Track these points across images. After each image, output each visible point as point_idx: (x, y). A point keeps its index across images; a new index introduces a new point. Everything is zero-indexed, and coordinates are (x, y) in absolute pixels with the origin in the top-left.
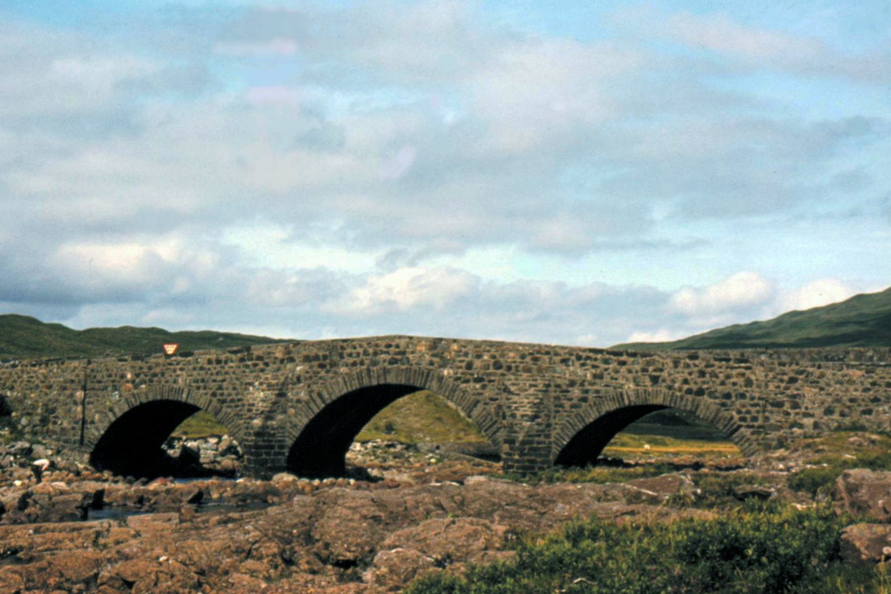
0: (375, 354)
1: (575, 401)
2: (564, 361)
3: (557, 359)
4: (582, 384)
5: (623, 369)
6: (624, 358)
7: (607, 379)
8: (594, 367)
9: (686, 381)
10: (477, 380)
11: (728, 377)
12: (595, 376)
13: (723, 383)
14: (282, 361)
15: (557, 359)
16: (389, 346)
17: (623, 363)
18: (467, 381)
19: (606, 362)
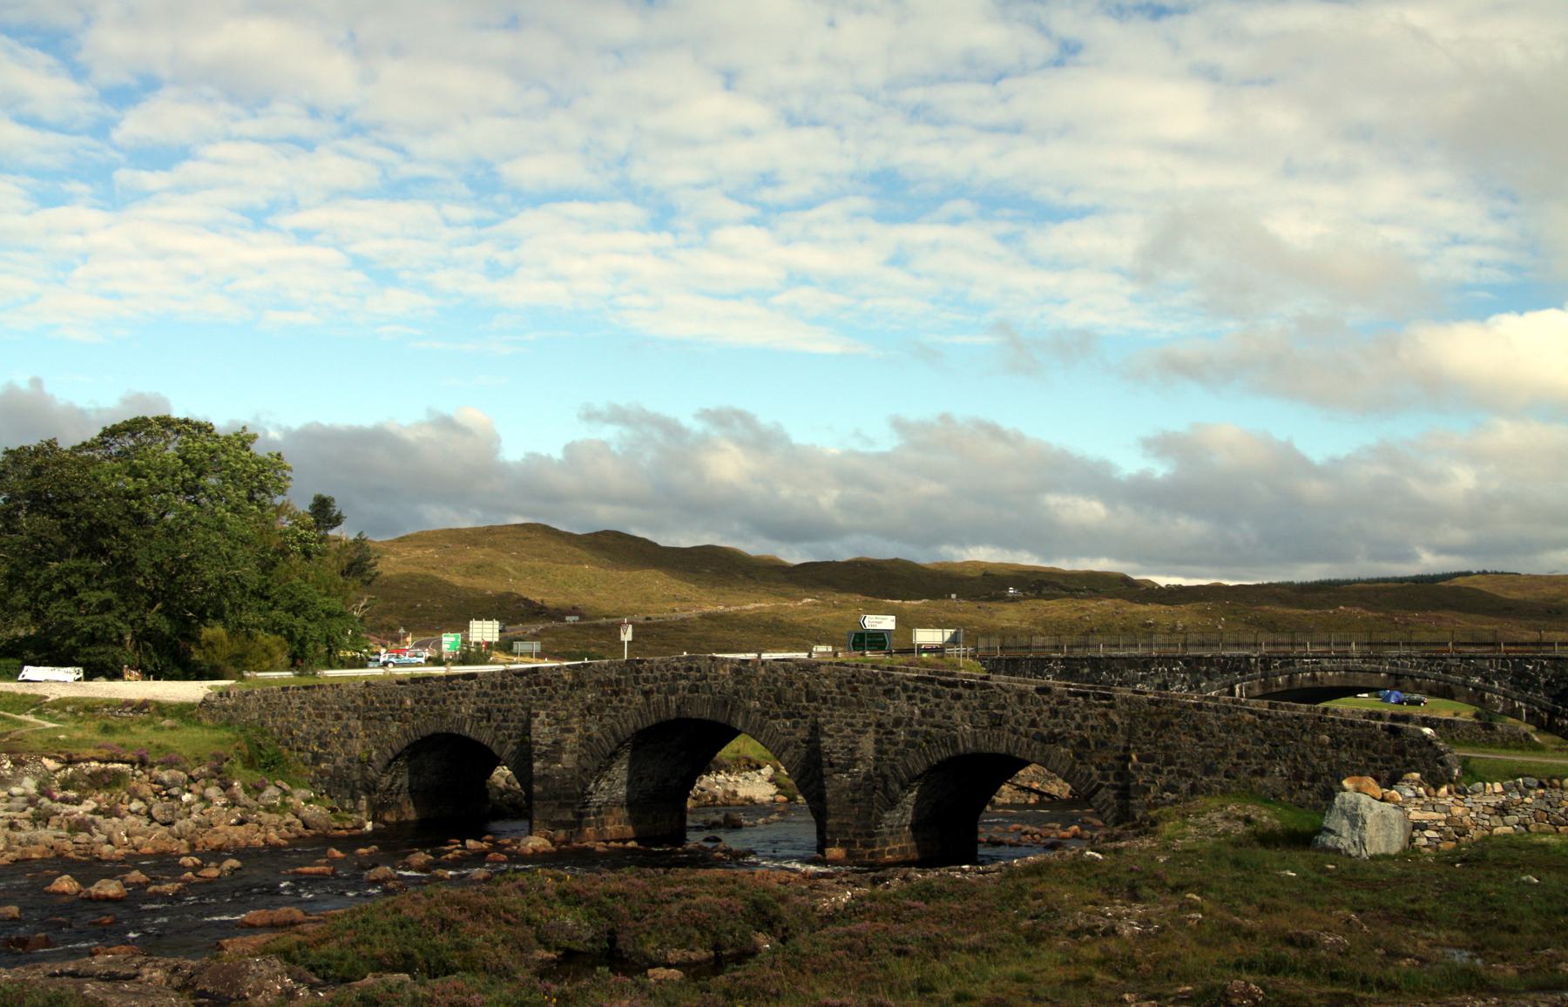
0: (675, 678)
1: (901, 746)
2: (888, 693)
3: (879, 689)
4: (909, 724)
5: (958, 705)
6: (960, 690)
7: (938, 717)
8: (923, 701)
9: (1033, 723)
10: (788, 716)
11: (1085, 718)
12: (923, 713)
13: (1079, 727)
14: (572, 687)
15: (879, 689)
16: (690, 669)
17: (958, 697)
18: (776, 717)
19: (937, 695)
